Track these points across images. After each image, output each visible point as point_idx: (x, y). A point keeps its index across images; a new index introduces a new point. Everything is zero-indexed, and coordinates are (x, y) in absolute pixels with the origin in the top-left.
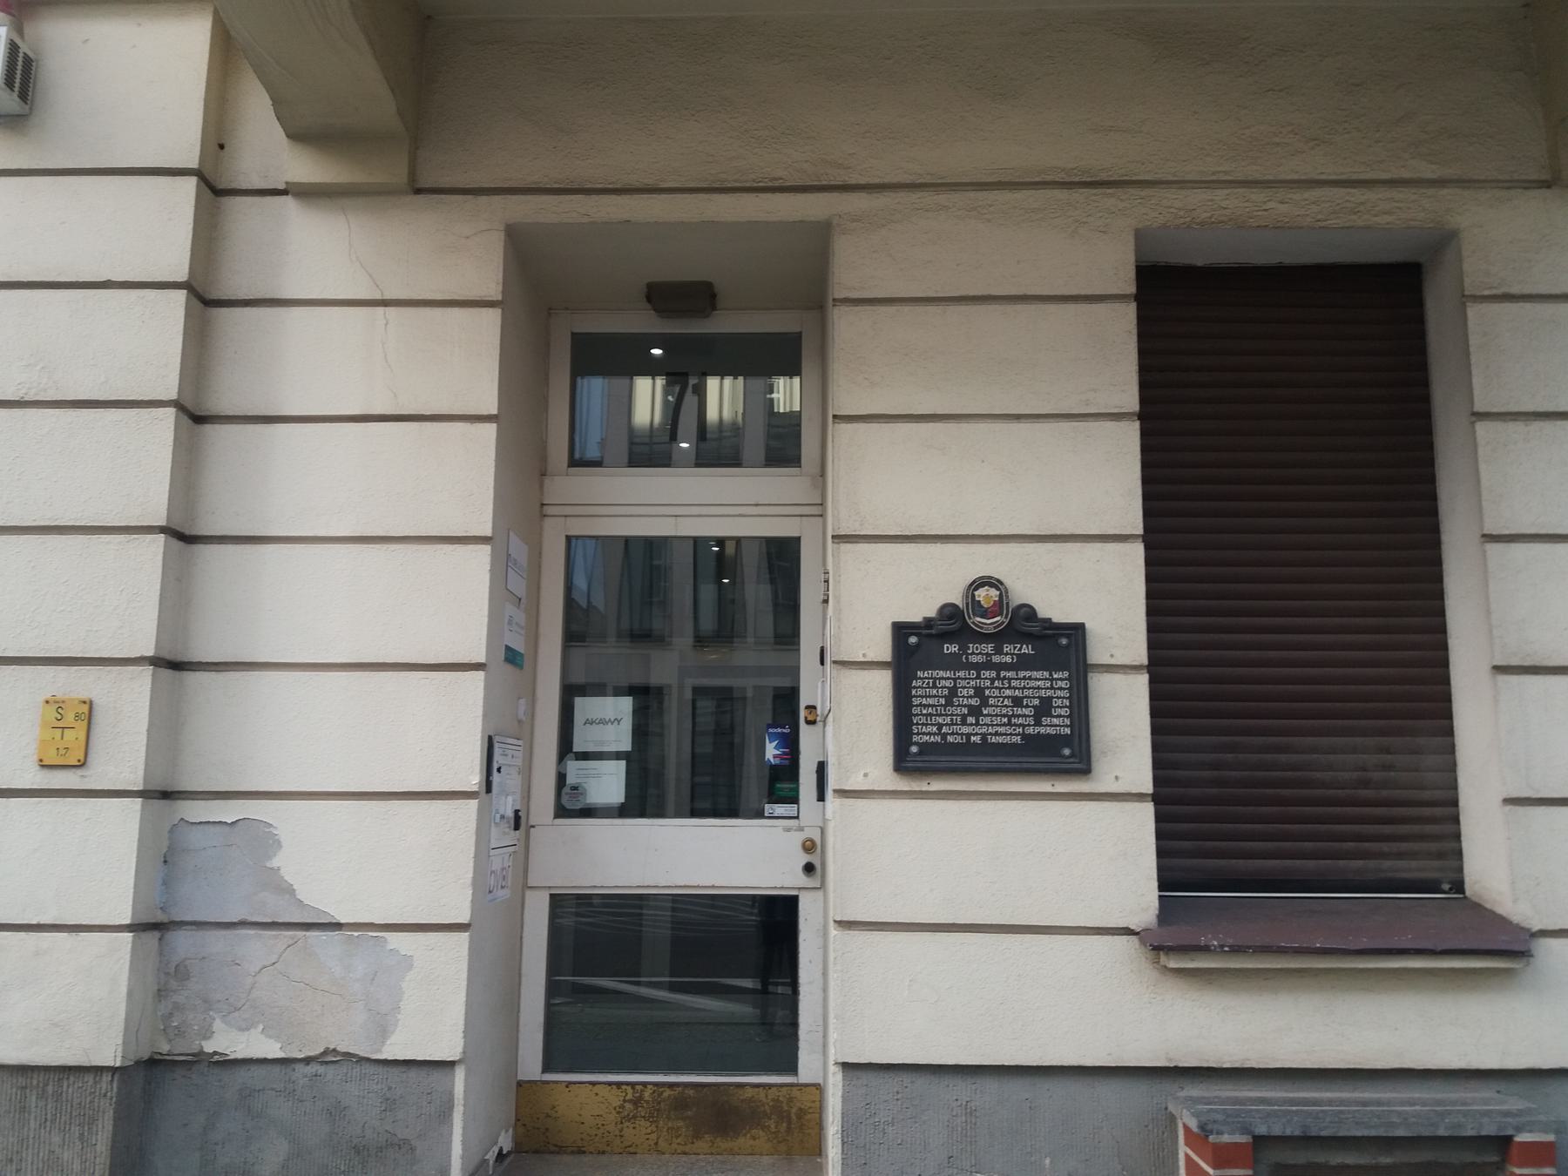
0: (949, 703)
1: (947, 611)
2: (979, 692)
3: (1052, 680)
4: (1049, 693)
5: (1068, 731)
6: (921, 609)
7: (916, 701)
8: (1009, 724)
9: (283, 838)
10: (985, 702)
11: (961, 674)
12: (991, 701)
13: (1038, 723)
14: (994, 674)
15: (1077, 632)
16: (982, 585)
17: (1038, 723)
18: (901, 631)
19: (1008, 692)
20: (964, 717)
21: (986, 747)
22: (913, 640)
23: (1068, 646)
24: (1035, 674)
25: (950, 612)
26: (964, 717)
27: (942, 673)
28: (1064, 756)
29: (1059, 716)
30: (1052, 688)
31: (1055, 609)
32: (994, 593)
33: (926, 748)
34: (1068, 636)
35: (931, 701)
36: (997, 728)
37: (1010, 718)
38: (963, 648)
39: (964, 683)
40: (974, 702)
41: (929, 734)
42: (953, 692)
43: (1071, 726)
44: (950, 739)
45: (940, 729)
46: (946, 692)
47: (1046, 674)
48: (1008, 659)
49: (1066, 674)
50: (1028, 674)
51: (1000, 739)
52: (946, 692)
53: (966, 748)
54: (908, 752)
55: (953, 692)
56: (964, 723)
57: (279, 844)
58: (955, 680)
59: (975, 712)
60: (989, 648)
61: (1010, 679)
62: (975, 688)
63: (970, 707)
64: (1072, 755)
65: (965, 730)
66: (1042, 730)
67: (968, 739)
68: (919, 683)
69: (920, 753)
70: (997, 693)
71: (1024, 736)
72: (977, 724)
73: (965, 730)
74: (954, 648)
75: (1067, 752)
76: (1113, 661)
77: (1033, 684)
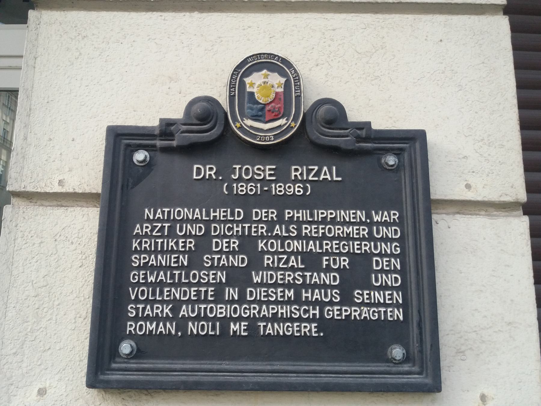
0: (195, 262)
1: (197, 109)
2: (247, 243)
3: (371, 224)
4: (366, 247)
5: (399, 314)
6: (157, 105)
7: (136, 260)
8: (298, 300)
9: (105, 129)
10: (256, 262)
11: (220, 213)
12: (267, 260)
13: (347, 300)
14: (273, 214)
15: (411, 144)
16: (247, 73)
17: (347, 300)
18: (121, 141)
19: (296, 245)
20: (219, 288)
21: (256, 345)
22: (140, 156)
23: (397, 169)
24: (342, 214)
25: (205, 112)
26: (219, 288)
27: (186, 212)
28: (391, 361)
29: (384, 288)
30: (371, 238)
31: (375, 107)
32: (276, 80)
33: (146, 347)
34: (398, 152)
35: (163, 260)
36: (276, 305)
37: (298, 290)
39: (221, 229)
40: (238, 261)
41: (157, 319)
42: (204, 243)
43: (405, 306)
44: (192, 328)
45: (175, 310)
46: (191, 244)
47: (361, 215)
48: (297, 189)
49: (395, 215)
50: (330, 214)
51: (280, 329)
52: (191, 244)
53: (221, 345)
54: (115, 353)
55: (204, 243)
56: (219, 298)
57: (192, 103)
58: (208, 223)
59: (239, 278)
60: (267, 171)
61: (299, 223)
62: (241, 237)
63: (230, 270)
64: (407, 359)
65: (221, 311)
66: (355, 313)
67: (225, 328)
68: (147, 228)
69: (138, 354)
70: (277, 245)
71: (322, 323)
72: (242, 300)
73: (221, 311)
74: (209, 171)
75: (397, 352)
76: (470, 196)
77: (338, 230)
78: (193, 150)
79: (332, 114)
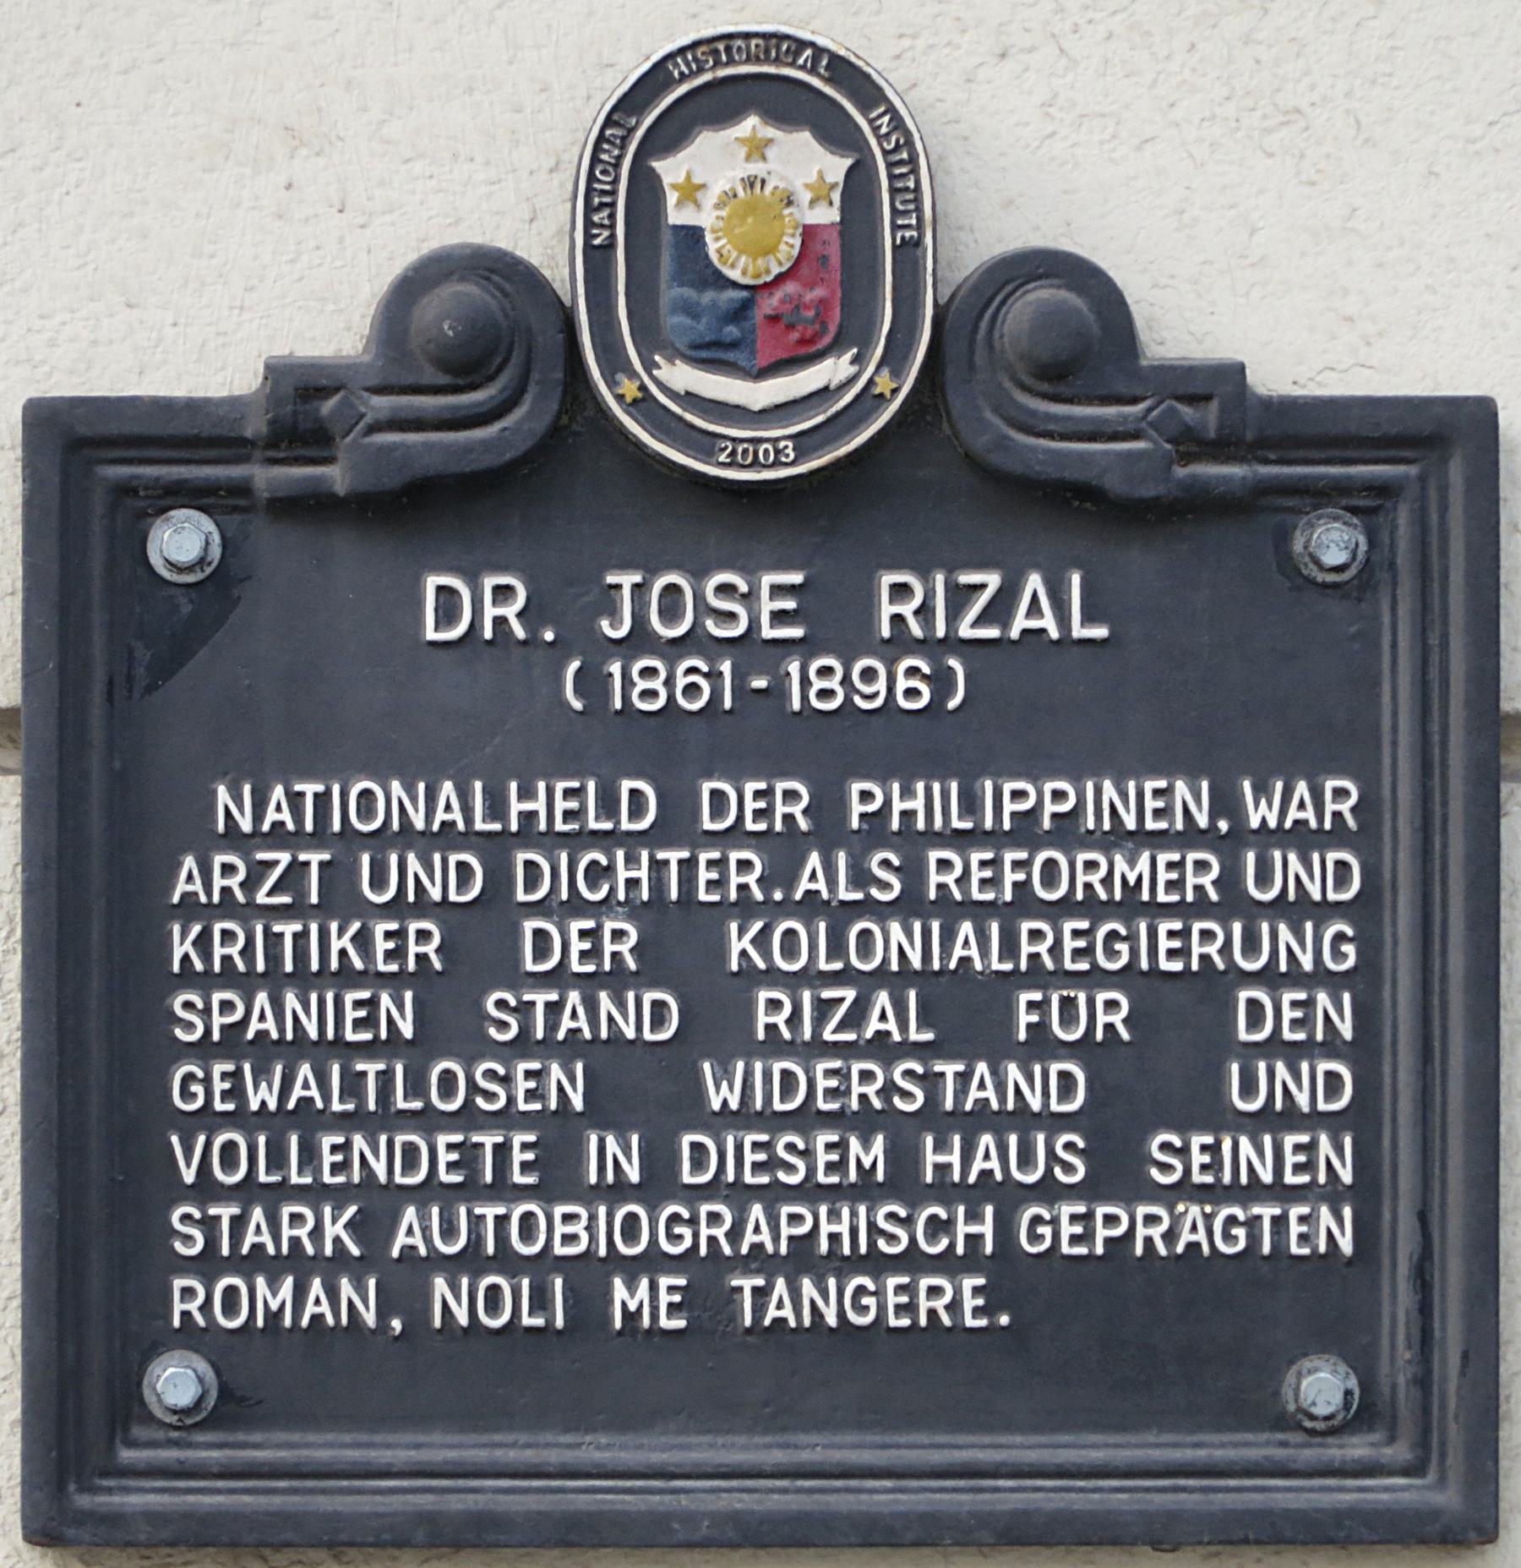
8: (903, 1181)
11: (547, 802)
32: (805, 166)
38: (566, 602)
40: (641, 1017)
48: (905, 685)
51: (824, 1301)
56: (557, 1175)
59: (644, 1090)
60: (759, 597)
63: (605, 1057)
65: (570, 1229)
66: (1148, 1227)
73: (570, 1229)
74: (497, 602)
78: (428, 509)
79: (1075, 323)
